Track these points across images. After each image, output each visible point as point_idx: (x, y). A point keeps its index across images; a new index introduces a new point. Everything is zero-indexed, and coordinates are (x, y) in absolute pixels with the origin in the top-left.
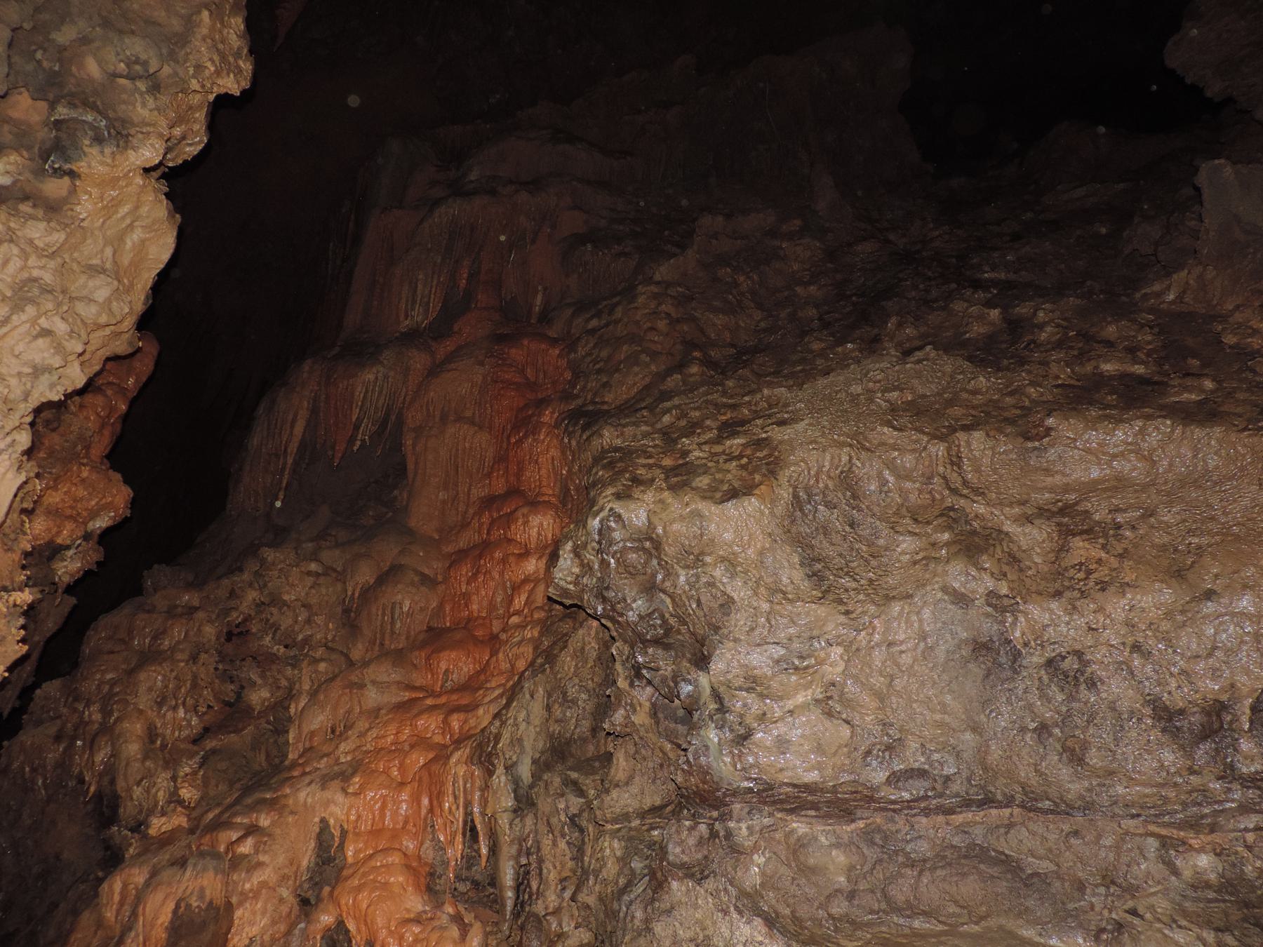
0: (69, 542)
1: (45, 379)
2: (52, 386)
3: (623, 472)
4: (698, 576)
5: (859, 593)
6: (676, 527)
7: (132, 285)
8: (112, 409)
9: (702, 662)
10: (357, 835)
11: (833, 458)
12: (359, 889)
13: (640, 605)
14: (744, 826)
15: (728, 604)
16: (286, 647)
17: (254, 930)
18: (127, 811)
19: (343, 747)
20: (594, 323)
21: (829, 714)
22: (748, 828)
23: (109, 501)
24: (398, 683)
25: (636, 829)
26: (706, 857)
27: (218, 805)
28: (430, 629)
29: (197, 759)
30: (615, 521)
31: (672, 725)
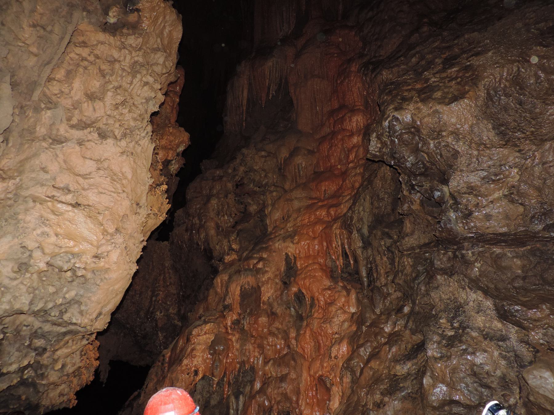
0: (172, 158)
1: (151, 103)
2: (154, 105)
3: (397, 95)
4: (439, 143)
5: (526, 140)
6: (426, 120)
7: (170, 52)
8: (174, 102)
9: (445, 181)
10: (300, 258)
11: (508, 70)
12: (305, 278)
13: (411, 159)
14: (470, 252)
15: (456, 154)
16: (259, 187)
17: (269, 294)
18: (216, 254)
19: (288, 225)
20: (370, 14)
21: (512, 201)
22: (472, 253)
23: (181, 139)
24: (306, 197)
25: (418, 253)
26: (452, 266)
27: (247, 250)
28: (315, 173)
29: (235, 233)
30: (396, 121)
31: (431, 208)
